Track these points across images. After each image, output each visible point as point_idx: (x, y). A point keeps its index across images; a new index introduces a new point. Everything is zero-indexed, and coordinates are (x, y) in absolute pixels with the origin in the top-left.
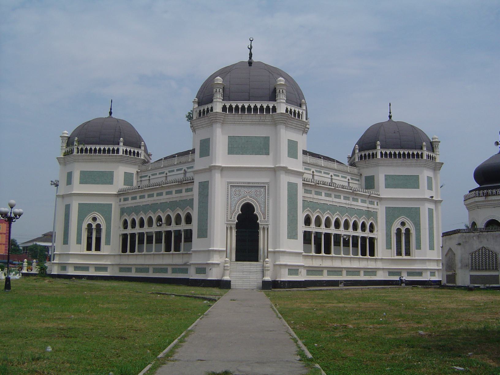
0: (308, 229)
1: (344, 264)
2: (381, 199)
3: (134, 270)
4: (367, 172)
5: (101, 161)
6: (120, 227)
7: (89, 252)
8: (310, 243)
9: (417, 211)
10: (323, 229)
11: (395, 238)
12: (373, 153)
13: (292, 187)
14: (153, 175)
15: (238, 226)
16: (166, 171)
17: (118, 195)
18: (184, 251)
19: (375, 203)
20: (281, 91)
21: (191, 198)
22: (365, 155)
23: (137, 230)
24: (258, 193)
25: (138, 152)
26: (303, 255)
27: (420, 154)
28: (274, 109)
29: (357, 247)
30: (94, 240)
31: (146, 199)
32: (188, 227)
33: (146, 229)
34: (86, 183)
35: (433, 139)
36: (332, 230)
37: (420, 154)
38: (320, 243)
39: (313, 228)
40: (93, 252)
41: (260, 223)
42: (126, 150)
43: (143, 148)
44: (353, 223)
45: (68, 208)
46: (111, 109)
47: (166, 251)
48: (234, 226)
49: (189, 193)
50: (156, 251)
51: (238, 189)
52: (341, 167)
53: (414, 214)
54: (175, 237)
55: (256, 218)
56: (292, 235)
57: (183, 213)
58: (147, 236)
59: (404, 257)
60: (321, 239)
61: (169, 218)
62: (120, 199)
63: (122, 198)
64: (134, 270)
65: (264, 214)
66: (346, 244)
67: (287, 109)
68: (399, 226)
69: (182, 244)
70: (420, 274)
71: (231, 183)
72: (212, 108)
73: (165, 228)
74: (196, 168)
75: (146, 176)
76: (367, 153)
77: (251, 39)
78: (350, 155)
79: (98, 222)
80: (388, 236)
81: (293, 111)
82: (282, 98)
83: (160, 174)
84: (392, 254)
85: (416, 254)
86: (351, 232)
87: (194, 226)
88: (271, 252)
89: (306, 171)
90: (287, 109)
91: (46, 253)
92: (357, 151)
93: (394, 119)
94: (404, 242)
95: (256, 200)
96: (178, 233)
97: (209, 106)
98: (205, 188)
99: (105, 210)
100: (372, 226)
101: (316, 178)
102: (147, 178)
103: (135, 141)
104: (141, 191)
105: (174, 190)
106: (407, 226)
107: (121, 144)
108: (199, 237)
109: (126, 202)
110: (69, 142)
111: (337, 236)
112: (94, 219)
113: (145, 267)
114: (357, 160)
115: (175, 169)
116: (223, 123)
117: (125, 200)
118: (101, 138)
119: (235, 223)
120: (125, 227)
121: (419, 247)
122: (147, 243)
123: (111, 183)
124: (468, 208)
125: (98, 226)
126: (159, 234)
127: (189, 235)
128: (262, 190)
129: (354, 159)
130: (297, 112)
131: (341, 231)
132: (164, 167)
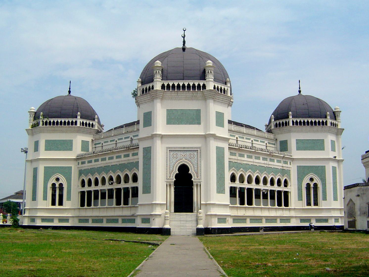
0: (233, 185)
1: (264, 213)
2: (293, 159)
3: (90, 221)
4: (281, 137)
6: (78, 186)
8: (235, 197)
10: (246, 185)
13: (220, 151)
16: (116, 139)
17: (77, 159)
20: (210, 71)
21: (137, 161)
22: (283, 122)
23: (93, 188)
27: (325, 122)
28: (204, 87)
29: (274, 199)
30: (57, 197)
31: (100, 162)
32: (135, 185)
33: (100, 187)
34: (50, 150)
36: (253, 186)
37: (325, 122)
38: (243, 196)
39: (237, 184)
41: (194, 181)
42: (83, 122)
43: (96, 120)
45: (35, 171)
46: (70, 89)
48: (172, 184)
51: (175, 153)
52: (259, 134)
55: (190, 176)
56: (220, 190)
57: (131, 174)
58: (101, 193)
59: (313, 207)
62: (79, 163)
63: (80, 161)
64: (90, 221)
65: (197, 173)
66: (265, 196)
67: (215, 86)
68: (54, 181)
70: (326, 220)
71: (170, 148)
72: (153, 86)
73: (115, 186)
75: (100, 143)
76: (281, 122)
77: (185, 29)
79: (60, 182)
80: (300, 189)
81: (223, 89)
82: (210, 77)
84: (303, 204)
85: (323, 204)
86: (269, 187)
87: (140, 184)
88: (203, 204)
89: (231, 138)
90: (215, 86)
92: (273, 120)
94: (312, 194)
97: (151, 85)
98: (148, 152)
99: (67, 172)
100: (286, 182)
101: (239, 142)
102: (101, 145)
103: (90, 115)
104: (96, 156)
106: (315, 181)
107: (79, 117)
108: (144, 193)
109: (83, 165)
110: (36, 116)
111: (258, 191)
112: (58, 179)
113: (99, 218)
114: (273, 128)
115: (123, 137)
116: (162, 99)
117: (83, 163)
118: (62, 113)
119: (173, 181)
120: (83, 184)
121: (325, 198)
123: (71, 149)
126: (111, 191)
127: (135, 192)
128: (195, 153)
129: (271, 127)
131: (261, 186)
132: (115, 135)
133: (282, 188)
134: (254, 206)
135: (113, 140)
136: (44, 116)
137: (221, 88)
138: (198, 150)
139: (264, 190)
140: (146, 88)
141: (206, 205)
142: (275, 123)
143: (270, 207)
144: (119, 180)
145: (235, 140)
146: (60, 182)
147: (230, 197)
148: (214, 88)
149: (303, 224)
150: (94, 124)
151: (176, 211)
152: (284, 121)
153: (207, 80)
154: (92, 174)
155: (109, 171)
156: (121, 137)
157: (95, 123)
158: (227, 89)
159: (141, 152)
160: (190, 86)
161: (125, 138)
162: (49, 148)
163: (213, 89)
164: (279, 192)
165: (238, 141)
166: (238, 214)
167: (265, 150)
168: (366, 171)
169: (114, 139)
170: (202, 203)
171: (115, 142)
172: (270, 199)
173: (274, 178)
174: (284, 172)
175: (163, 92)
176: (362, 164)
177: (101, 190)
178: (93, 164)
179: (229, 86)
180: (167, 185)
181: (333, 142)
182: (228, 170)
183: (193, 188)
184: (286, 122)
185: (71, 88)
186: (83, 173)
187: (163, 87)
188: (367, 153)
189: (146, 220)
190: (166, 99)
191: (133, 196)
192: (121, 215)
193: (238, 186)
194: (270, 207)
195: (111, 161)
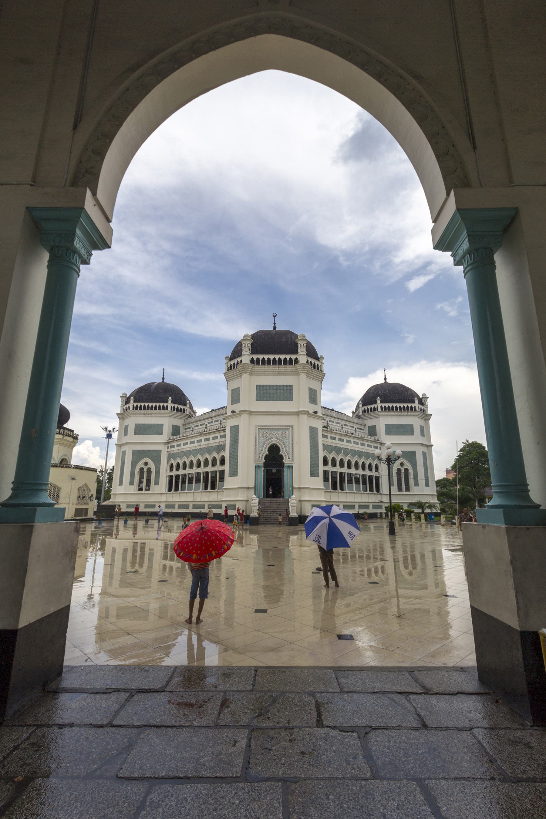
0: (326, 468)
4: (370, 422)
7: (140, 492)
9: (413, 453)
10: (338, 469)
11: (396, 478)
12: (374, 407)
13: (313, 431)
14: (195, 426)
15: (266, 465)
16: (206, 423)
17: (166, 443)
22: (368, 409)
23: (181, 472)
24: (284, 435)
25: (184, 409)
28: (296, 361)
29: (366, 484)
30: (145, 480)
31: (189, 445)
33: (187, 471)
36: (345, 470)
38: (336, 482)
39: (330, 468)
40: (144, 492)
41: (285, 462)
42: (174, 407)
45: (124, 453)
46: (275, 324)
49: (223, 439)
50: (188, 490)
53: (411, 456)
55: (282, 457)
56: (314, 473)
60: (336, 477)
61: (206, 461)
63: (169, 445)
65: (288, 454)
66: (357, 481)
71: (259, 426)
73: (203, 469)
77: (275, 315)
79: (148, 466)
82: (302, 351)
83: (201, 425)
84: (133, 489)
85: (414, 490)
86: (360, 472)
88: (296, 488)
91: (487, 500)
92: (361, 406)
93: (387, 381)
99: (155, 455)
102: (191, 429)
107: (170, 401)
108: (230, 476)
111: (349, 475)
112: (146, 464)
113: (171, 503)
114: (361, 413)
116: (251, 374)
117: (172, 447)
120: (383, 568)
121: (416, 484)
122: (196, 483)
125: (149, 470)
129: (359, 413)
130: (316, 364)
131: (353, 471)
132: (204, 419)
133: (374, 473)
136: (135, 402)
137: (314, 364)
139: (356, 474)
141: (299, 488)
142: (363, 408)
146: (148, 466)
147: (324, 481)
148: (307, 362)
151: (385, 425)
152: (372, 406)
153: (300, 353)
157: (187, 408)
164: (370, 477)
171: (205, 426)
181: (422, 428)
187: (252, 361)
189: (68, 493)
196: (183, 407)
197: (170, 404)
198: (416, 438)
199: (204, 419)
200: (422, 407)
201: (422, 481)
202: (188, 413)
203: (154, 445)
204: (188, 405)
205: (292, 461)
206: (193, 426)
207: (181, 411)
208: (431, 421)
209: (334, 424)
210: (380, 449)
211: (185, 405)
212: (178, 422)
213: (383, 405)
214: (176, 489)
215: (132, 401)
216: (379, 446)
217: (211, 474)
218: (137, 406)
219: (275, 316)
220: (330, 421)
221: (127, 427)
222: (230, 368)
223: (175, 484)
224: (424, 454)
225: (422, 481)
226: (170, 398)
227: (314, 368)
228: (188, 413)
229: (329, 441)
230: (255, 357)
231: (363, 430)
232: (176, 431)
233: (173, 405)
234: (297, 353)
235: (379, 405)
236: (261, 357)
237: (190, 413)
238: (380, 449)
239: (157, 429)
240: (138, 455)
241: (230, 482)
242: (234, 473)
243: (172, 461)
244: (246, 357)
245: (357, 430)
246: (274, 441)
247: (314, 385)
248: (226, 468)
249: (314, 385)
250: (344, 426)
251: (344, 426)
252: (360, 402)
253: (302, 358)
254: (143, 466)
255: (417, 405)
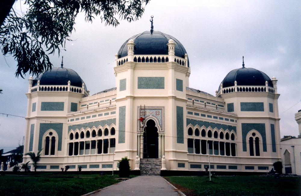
0: (191, 137)
1: (212, 160)
2: (238, 118)
4: (228, 101)
5: (243, 96)
8: (192, 147)
10: (200, 138)
14: (90, 104)
16: (99, 101)
18: (110, 153)
19: (235, 121)
20: (171, 48)
21: (114, 118)
23: (80, 140)
24: (158, 113)
25: (80, 90)
26: (188, 155)
27: (264, 88)
28: (167, 60)
29: (218, 149)
32: (113, 137)
33: (85, 139)
34: (45, 110)
35: (272, 79)
36: (207, 138)
37: (264, 88)
39: (194, 137)
40: (255, 156)
41: (159, 133)
42: (73, 88)
44: (220, 133)
45: (33, 126)
46: (62, 62)
47: (98, 154)
49: (114, 115)
53: (59, 127)
54: (104, 144)
56: (180, 139)
58: (86, 144)
59: (255, 156)
65: (161, 127)
67: (175, 59)
68: (48, 135)
69: (109, 149)
70: (252, 168)
72: (127, 59)
73: (97, 138)
74: (118, 98)
75: (86, 105)
77: (152, 17)
78: (217, 90)
79: (53, 135)
81: (179, 61)
82: (171, 52)
84: (247, 154)
85: (263, 154)
89: (189, 100)
90: (175, 59)
92: (221, 87)
95: (156, 118)
96: (106, 141)
99: (59, 127)
101: (195, 104)
102: (86, 106)
103: (77, 82)
104: (82, 115)
105: (103, 113)
106: (257, 136)
107: (69, 84)
108: (120, 142)
109: (78, 121)
112: (51, 134)
115: (104, 100)
121: (265, 150)
124: (298, 123)
125: (54, 138)
126: (94, 142)
127: (113, 141)
128: (160, 111)
129: (220, 93)
130: (182, 61)
132: (97, 99)
133: (230, 141)
134: (207, 154)
135: (97, 103)
136: (41, 84)
137: (180, 61)
138: (162, 109)
140: (122, 61)
142: (223, 89)
143: (214, 155)
144: (94, 134)
145: (192, 102)
146: (53, 135)
148: (175, 60)
149: (218, 170)
150: (81, 90)
152: (231, 88)
153: (169, 54)
154: (91, 127)
155: (93, 126)
156: (215, 103)
158: (185, 62)
159: (117, 111)
160: (141, 60)
161: (106, 101)
162: (44, 108)
163: (133, 61)
164: (228, 144)
165: (194, 103)
166: (90, 161)
167: (215, 111)
168: (299, 127)
169: (97, 101)
170: (165, 150)
172: (214, 149)
173: (223, 133)
174: (231, 128)
175: (134, 63)
176: (296, 121)
177: (86, 142)
178: (80, 121)
179: (187, 59)
180: (138, 136)
182: (186, 126)
183: (158, 139)
184: (232, 89)
185: (63, 62)
186: (71, 128)
187: (135, 60)
188: (300, 112)
190: (138, 69)
191: (111, 147)
192: (78, 162)
193: (201, 139)
194: (214, 155)
195: (94, 118)
196: (79, 88)
197: (69, 86)
198: (266, 113)
199: (97, 99)
200: (271, 88)
201: (269, 147)
202: (83, 93)
203: (59, 119)
204: (83, 87)
205: (164, 132)
206: (88, 104)
207: (78, 91)
208: (280, 100)
209: (199, 102)
210: (236, 122)
211: (81, 86)
212: (75, 100)
213: (239, 87)
214: (76, 153)
215: (38, 84)
216: (235, 120)
217: (80, 143)
218: (43, 88)
219: (152, 18)
220: (195, 100)
221: (34, 105)
222: (120, 63)
223: (74, 149)
224: (272, 127)
225: (269, 147)
226: (69, 81)
227: (180, 64)
228: (83, 93)
229: (193, 117)
230: (137, 56)
231: (223, 106)
232: (74, 107)
233: (72, 87)
234: (168, 54)
235: (236, 87)
236: (141, 56)
237: (85, 93)
238: (236, 122)
239: (59, 106)
240: (44, 127)
241: (119, 146)
242: (122, 140)
243: (72, 131)
244: (130, 57)
245: (218, 107)
246: (151, 118)
247: (182, 76)
248: (116, 136)
249: (182, 76)
250: (207, 104)
251: (207, 104)
252: (221, 84)
253: (171, 56)
254: (252, 136)
255: (267, 86)
